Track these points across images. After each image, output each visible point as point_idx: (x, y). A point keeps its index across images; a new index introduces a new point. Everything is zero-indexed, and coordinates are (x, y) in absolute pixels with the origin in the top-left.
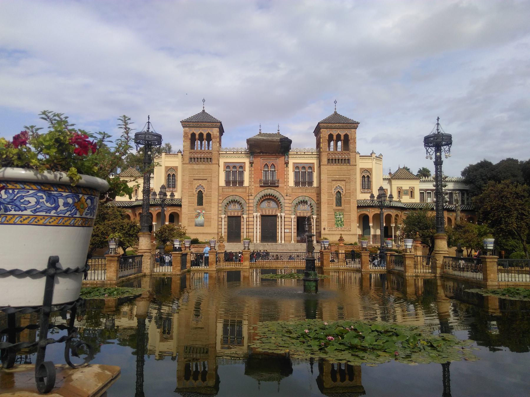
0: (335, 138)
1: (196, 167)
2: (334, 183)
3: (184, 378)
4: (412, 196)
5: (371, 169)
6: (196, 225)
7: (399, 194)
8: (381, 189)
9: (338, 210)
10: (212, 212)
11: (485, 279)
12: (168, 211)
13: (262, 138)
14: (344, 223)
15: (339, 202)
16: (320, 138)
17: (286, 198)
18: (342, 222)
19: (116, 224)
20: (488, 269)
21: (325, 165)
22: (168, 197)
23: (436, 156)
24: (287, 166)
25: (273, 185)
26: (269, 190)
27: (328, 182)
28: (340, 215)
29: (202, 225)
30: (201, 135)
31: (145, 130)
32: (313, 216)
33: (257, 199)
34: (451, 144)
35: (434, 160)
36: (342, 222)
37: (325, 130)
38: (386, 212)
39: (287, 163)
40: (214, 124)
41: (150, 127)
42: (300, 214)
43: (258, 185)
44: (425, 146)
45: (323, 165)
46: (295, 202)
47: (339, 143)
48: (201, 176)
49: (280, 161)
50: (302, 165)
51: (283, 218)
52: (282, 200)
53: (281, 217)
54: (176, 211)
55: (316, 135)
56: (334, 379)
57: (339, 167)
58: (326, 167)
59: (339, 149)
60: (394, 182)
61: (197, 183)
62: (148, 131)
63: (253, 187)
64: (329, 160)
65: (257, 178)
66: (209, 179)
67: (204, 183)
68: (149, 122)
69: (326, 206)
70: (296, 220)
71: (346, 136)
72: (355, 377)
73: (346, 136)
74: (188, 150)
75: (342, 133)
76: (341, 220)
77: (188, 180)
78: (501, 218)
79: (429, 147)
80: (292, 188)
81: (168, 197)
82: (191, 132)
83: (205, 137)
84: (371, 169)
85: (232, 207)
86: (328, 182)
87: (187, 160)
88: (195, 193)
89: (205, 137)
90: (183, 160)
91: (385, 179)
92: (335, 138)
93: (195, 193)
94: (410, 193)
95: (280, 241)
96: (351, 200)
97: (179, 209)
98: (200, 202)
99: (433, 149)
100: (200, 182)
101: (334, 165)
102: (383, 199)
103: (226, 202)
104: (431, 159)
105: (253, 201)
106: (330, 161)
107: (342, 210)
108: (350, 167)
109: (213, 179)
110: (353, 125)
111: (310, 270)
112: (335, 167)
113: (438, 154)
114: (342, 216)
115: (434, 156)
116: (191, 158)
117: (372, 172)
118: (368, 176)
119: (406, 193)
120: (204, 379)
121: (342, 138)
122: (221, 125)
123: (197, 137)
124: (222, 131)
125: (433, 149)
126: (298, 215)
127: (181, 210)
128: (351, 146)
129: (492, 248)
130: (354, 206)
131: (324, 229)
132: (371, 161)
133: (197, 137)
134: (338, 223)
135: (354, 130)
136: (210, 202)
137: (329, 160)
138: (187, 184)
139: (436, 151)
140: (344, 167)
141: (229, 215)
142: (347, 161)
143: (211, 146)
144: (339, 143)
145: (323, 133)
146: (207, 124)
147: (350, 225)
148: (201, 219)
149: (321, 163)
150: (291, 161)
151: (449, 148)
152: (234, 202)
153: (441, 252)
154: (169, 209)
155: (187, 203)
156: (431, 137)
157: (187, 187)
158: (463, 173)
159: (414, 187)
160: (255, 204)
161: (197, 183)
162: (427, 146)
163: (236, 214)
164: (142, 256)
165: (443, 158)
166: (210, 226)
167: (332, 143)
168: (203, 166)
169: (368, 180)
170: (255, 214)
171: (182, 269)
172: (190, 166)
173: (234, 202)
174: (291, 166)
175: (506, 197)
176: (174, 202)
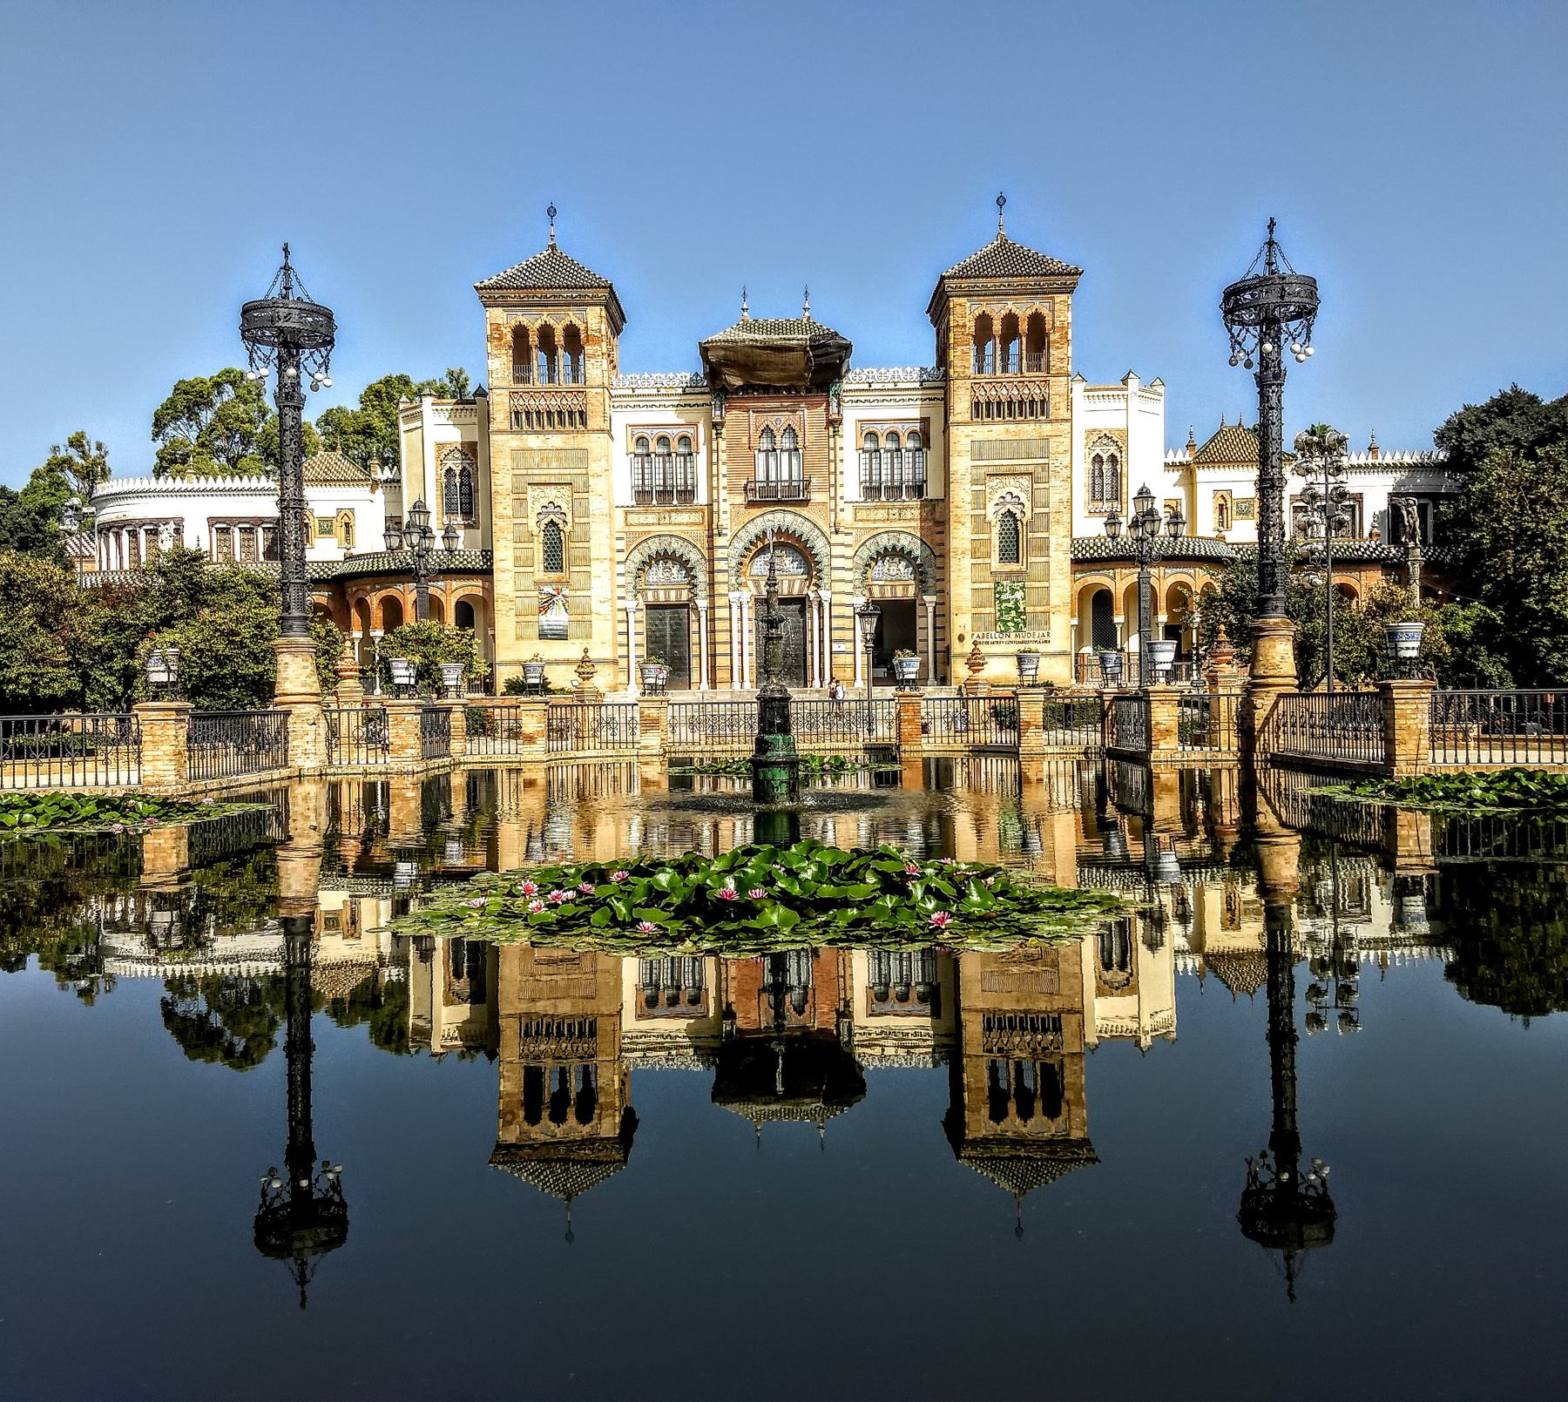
0: (997, 327)
1: (533, 441)
2: (995, 482)
3: (522, 1114)
6: (543, 636)
7: (1221, 513)
9: (1009, 574)
11: (1390, 758)
12: (451, 593)
13: (751, 336)
14: (1029, 618)
15: (1012, 548)
16: (948, 329)
17: (835, 539)
18: (1019, 614)
19: (238, 621)
20: (1399, 722)
21: (966, 424)
25: (794, 497)
26: (779, 516)
27: (975, 482)
28: (1013, 591)
29: (561, 636)
30: (546, 333)
33: (739, 545)
35: (1256, 369)
36: (1019, 614)
38: (1164, 579)
39: (834, 424)
40: (590, 292)
43: (740, 499)
45: (959, 424)
46: (865, 553)
48: (553, 472)
49: (809, 417)
50: (887, 427)
51: (826, 605)
52: (819, 546)
53: (820, 605)
56: (998, 1114)
57: (1012, 427)
58: (968, 430)
60: (1202, 474)
61: (537, 499)
64: (977, 404)
65: (739, 475)
66: (579, 482)
67: (561, 496)
68: (286, 268)
69: (967, 561)
71: (1037, 320)
72: (1064, 1107)
73: (1037, 320)
75: (1023, 309)
76: (1016, 608)
78: (1529, 573)
81: (439, 544)
85: (657, 574)
86: (975, 482)
88: (535, 530)
91: (1174, 465)
93: (535, 530)
95: (817, 683)
96: (1052, 539)
98: (554, 560)
99: (1255, 331)
100: (552, 492)
101: (994, 423)
102: (1148, 527)
104: (1248, 365)
107: (1021, 572)
108: (1047, 429)
109: (592, 481)
110: (1061, 280)
111: (770, 733)
112: (998, 430)
114: (1019, 595)
115: (1255, 358)
116: (517, 413)
118: (1113, 458)
120: (584, 1117)
121: (1023, 327)
122: (612, 293)
126: (877, 594)
129: (1414, 654)
130: (1060, 560)
132: (1122, 405)
134: (1005, 617)
136: (587, 561)
137: (977, 404)
138: (509, 500)
140: (1029, 430)
141: (650, 597)
145: (958, 310)
146: (566, 293)
147: (1047, 622)
148: (557, 617)
149: (952, 419)
150: (851, 416)
152: (665, 557)
153: (1270, 680)
154: (455, 584)
155: (509, 564)
158: (1441, 438)
161: (537, 499)
164: (288, 713)
165: (1287, 360)
168: (556, 441)
169: (1115, 474)
170: (733, 596)
171: (427, 756)
173: (665, 557)
174: (849, 429)
175: (1548, 503)
176: (456, 563)
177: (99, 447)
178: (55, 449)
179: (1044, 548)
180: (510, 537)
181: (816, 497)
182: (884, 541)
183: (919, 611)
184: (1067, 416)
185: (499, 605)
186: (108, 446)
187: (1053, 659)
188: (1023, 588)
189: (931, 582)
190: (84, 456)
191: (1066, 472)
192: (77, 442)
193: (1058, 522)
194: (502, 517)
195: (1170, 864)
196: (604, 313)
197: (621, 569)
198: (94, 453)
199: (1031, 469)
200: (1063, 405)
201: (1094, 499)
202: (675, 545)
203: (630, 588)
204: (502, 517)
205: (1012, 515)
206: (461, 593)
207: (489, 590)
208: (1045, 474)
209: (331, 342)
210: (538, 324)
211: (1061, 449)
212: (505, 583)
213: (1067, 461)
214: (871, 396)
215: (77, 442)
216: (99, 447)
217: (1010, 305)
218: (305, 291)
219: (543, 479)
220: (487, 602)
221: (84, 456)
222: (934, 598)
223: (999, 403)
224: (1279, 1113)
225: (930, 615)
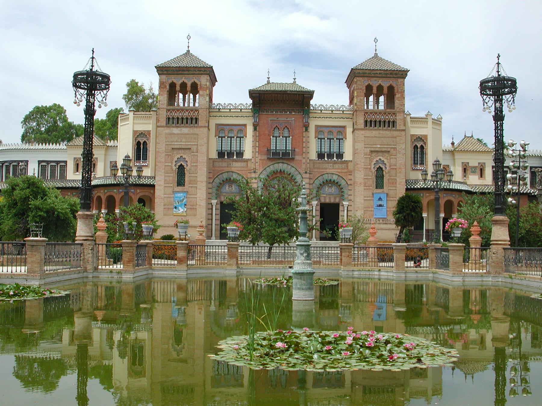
0: (375, 90)
1: (175, 131)
4: (481, 177)
5: (426, 136)
8: (437, 164)
10: (198, 195)
21: (361, 129)
22: (135, 173)
23: (496, 108)
24: (306, 130)
26: (281, 165)
31: (88, 68)
32: (344, 203)
34: (515, 92)
35: (493, 113)
37: (361, 79)
41: (95, 64)
42: (325, 200)
43: (265, 157)
44: (481, 94)
47: (382, 99)
48: (183, 144)
54: (147, 194)
55: (349, 87)
57: (381, 132)
59: (382, 107)
62: (91, 70)
63: (257, 160)
66: (194, 148)
68: (93, 58)
69: (362, 188)
70: (319, 208)
74: (165, 106)
77: (164, 149)
79: (487, 95)
80: (214, 160)
82: (170, 81)
83: (189, 88)
84: (426, 136)
87: (163, 122)
88: (174, 168)
89: (189, 88)
90: (158, 120)
92: (375, 90)
94: (478, 171)
96: (398, 180)
97: (152, 191)
98: (181, 182)
103: (217, 181)
108: (396, 133)
112: (374, 133)
113: (498, 105)
115: (493, 109)
117: (427, 140)
119: (474, 170)
123: (178, 88)
124: (213, 80)
125: (492, 98)
126: (323, 201)
127: (154, 194)
128: (397, 102)
133: (178, 88)
135: (402, 80)
136: (195, 182)
138: (164, 155)
139: (496, 101)
142: (393, 124)
143: (197, 101)
144: (382, 99)
150: (313, 123)
151: (513, 98)
155: (162, 183)
156: (488, 82)
157: (163, 160)
159: (485, 163)
162: (484, 94)
166: (195, 215)
167: (371, 98)
168: (185, 130)
172: (167, 131)
180: (163, 171)
181: (297, 157)
183: (341, 208)
184: (404, 128)
187: (387, 231)
191: (403, 152)
193: (400, 172)
194: (160, 162)
195: (120, 273)
196: (209, 78)
197: (210, 186)
199: (389, 150)
200: (402, 123)
203: (214, 194)
204: (160, 162)
205: (382, 169)
206: (141, 194)
208: (395, 152)
209: (109, 88)
211: (402, 142)
212: (159, 192)
213: (403, 147)
217: (380, 82)
218: (99, 67)
219: (178, 147)
225: (314, 210)
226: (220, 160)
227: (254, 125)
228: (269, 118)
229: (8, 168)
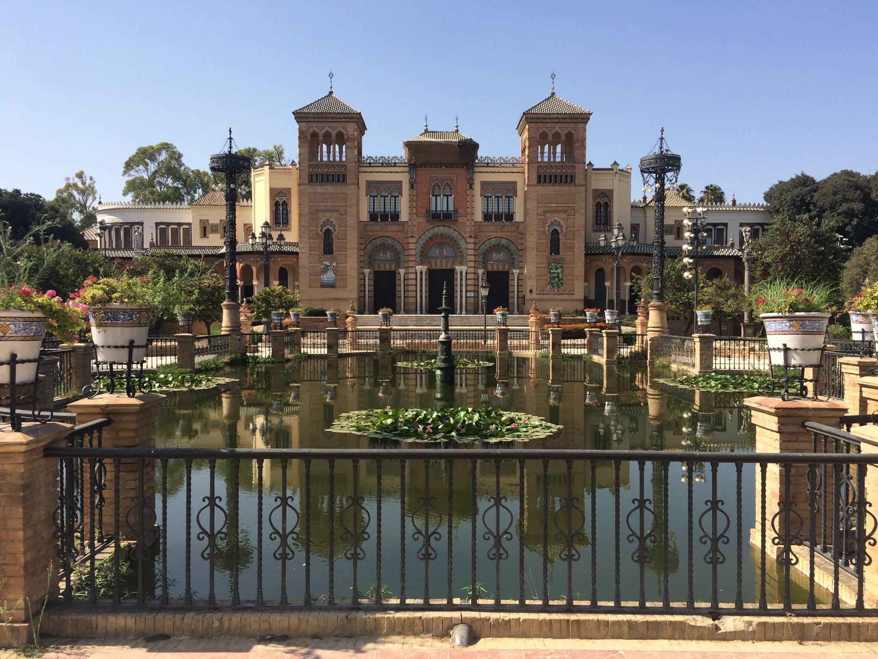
1: (320, 189)
18: (559, 280)
26: (442, 228)
33: (422, 242)
51: (464, 274)
57: (557, 188)
76: (558, 277)
77: (307, 211)
82: (311, 131)
86: (538, 214)
98: (328, 249)
100: (328, 214)
103: (370, 247)
105: (414, 247)
106: (314, 178)
108: (574, 189)
114: (559, 271)
126: (490, 269)
131: (531, 291)
134: (553, 281)
138: (307, 218)
150: (480, 178)
157: (307, 224)
160: (418, 251)
163: (388, 268)
168: (330, 188)
170: (419, 268)
172: (310, 189)
177: (91, 179)
178: (68, 179)
179: (572, 248)
182: (493, 241)
183: (511, 277)
184: (584, 183)
185: (300, 270)
186: (95, 178)
188: (562, 267)
189: (516, 263)
190: (84, 183)
192: (80, 175)
196: (356, 127)
198: (88, 182)
201: (597, 224)
202: (389, 241)
207: (297, 263)
210: (324, 131)
214: (514, 170)
215: (80, 175)
216: (91, 179)
220: (295, 270)
221: (84, 183)
222: (518, 271)
223: (545, 176)
224: (451, 467)
226: (486, 223)
227: (410, 182)
228: (426, 175)
229: (118, 232)
